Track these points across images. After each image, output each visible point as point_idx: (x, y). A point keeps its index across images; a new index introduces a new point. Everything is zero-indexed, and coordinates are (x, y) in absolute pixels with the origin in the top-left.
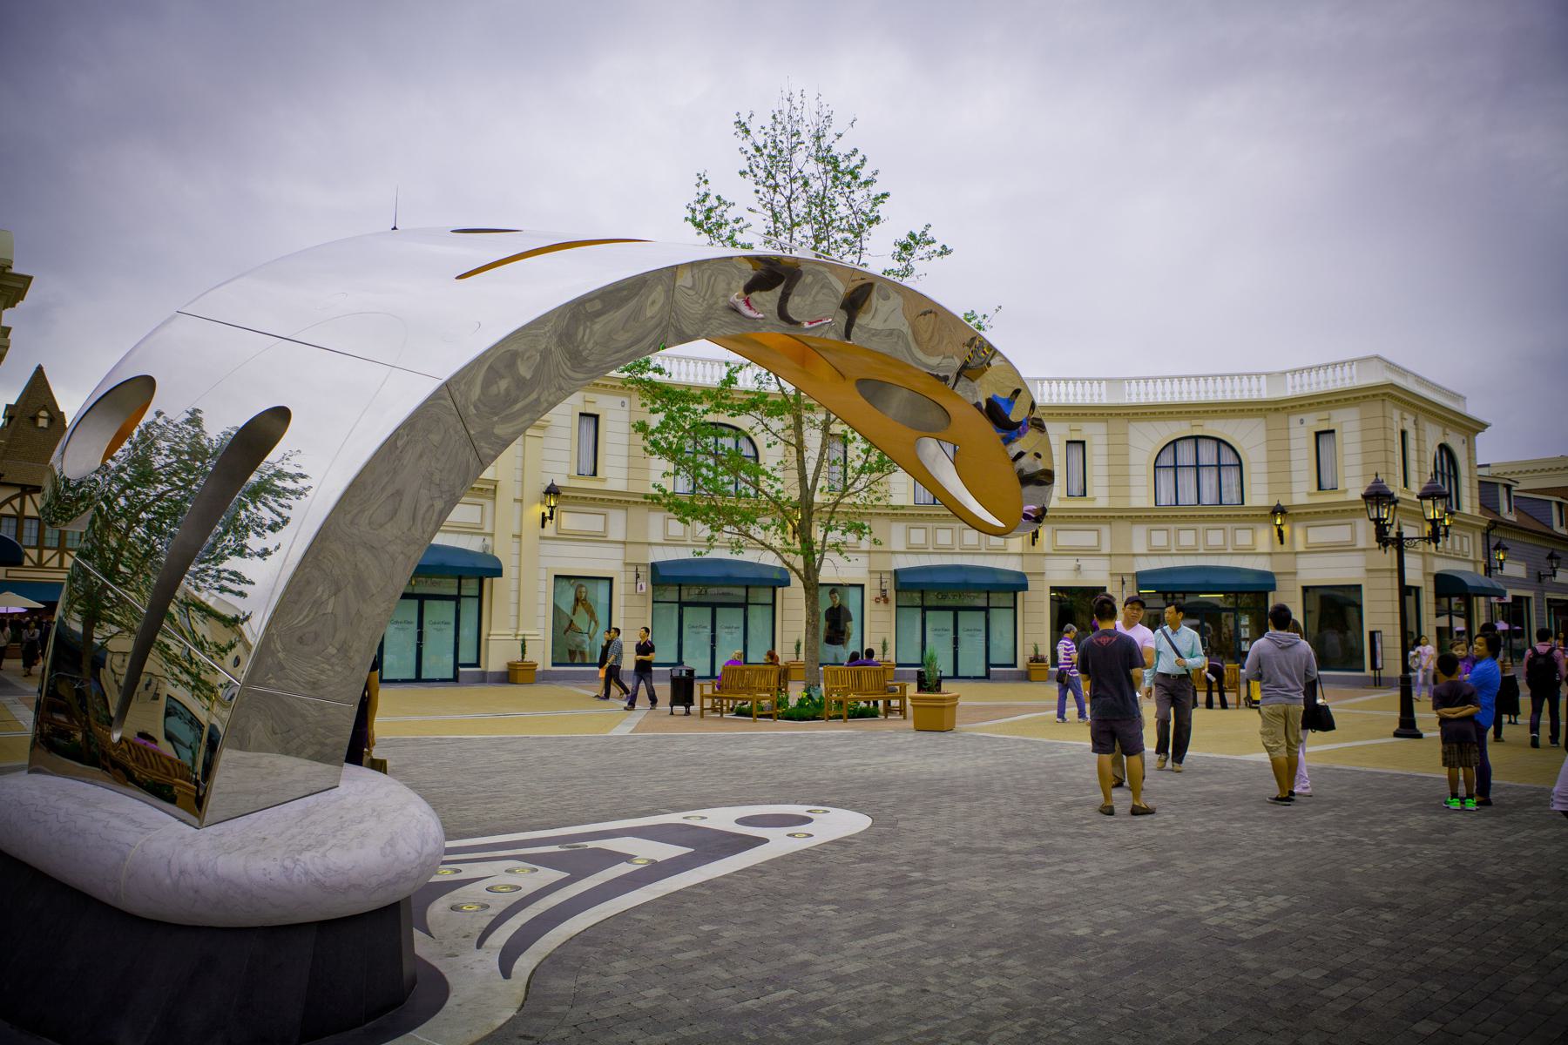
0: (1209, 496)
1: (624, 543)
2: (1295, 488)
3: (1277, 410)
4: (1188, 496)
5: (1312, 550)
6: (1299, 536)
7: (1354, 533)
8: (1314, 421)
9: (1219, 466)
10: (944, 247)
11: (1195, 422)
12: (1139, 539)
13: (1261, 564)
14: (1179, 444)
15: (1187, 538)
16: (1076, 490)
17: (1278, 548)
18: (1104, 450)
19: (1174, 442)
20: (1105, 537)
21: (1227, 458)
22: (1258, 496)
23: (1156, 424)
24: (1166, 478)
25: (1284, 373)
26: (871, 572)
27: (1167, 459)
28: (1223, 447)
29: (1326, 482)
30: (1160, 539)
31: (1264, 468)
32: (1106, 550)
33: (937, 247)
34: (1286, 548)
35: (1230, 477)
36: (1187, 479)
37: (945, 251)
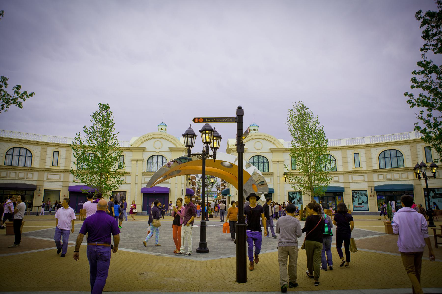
1: (37, 181)
5: (354, 182)
7: (60, 177)
12: (375, 177)
16: (358, 166)
20: (366, 177)
21: (28, 154)
23: (8, 143)
30: (381, 177)
32: (62, 180)
35: (28, 159)
36: (388, 160)
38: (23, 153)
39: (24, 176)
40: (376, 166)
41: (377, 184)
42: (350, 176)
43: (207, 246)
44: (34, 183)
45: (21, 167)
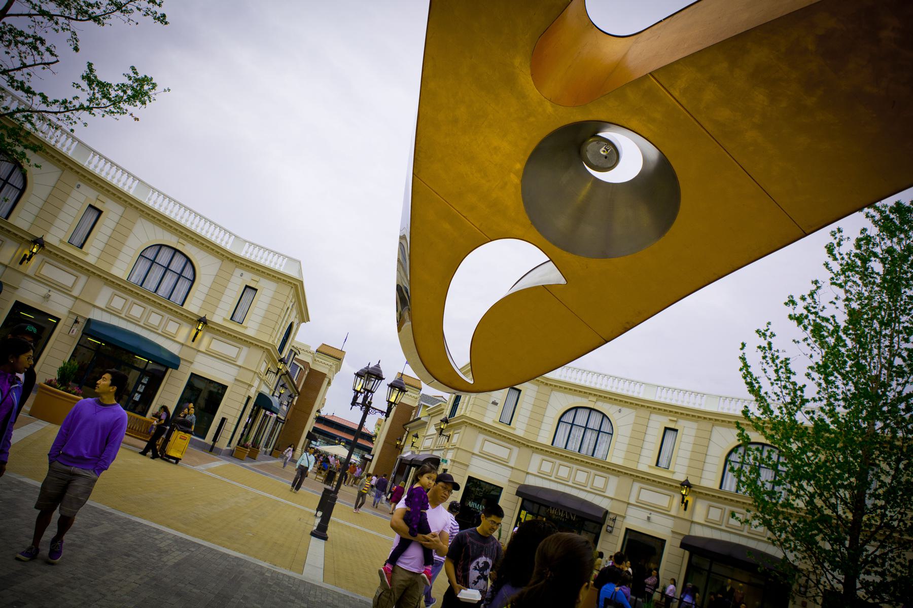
0: (164, 290)
2: (218, 311)
3: (232, 260)
4: (151, 284)
5: (209, 353)
6: (206, 341)
7: (238, 354)
8: (248, 278)
9: (180, 275)
10: (164, 16)
11: (181, 241)
12: (536, 463)
13: (174, 349)
14: (163, 249)
15: (564, 472)
17: (190, 343)
18: (112, 225)
19: (161, 246)
20: (514, 455)
21: (188, 273)
22: (194, 306)
24: (143, 266)
25: (246, 242)
26: (70, 312)
27: (150, 254)
28: (189, 265)
29: (238, 317)
30: (547, 467)
31: (627, 440)
33: (160, 11)
34: (194, 345)
35: (183, 286)
37: (162, 19)
38: (595, 421)
39: (570, 475)
40: (545, 438)
41: (532, 481)
42: (481, 437)
43: (327, 532)
44: (604, 504)
45: (174, 304)
